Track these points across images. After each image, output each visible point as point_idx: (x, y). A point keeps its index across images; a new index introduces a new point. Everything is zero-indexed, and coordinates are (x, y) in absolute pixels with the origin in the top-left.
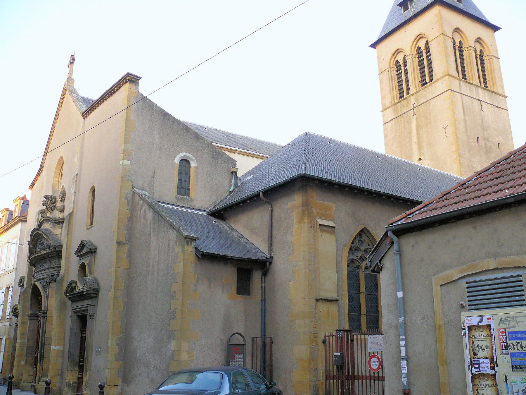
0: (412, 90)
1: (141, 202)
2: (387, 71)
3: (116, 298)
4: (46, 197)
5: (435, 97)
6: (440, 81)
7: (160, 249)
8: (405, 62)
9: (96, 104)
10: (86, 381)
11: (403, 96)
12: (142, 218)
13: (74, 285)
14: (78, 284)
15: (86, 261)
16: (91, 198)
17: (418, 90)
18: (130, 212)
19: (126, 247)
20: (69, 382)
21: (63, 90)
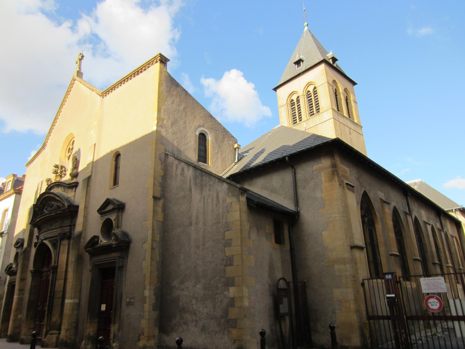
0: (304, 117)
1: (176, 162)
2: (285, 105)
3: (153, 249)
4: (57, 166)
5: (322, 123)
6: (325, 112)
7: (206, 202)
8: (298, 101)
9: (110, 90)
10: (114, 334)
11: (296, 122)
12: (179, 176)
13: (96, 240)
14: (101, 238)
15: (113, 217)
16: (114, 163)
17: (308, 118)
18: (163, 172)
19: (161, 202)
20: (89, 334)
21: (72, 81)
